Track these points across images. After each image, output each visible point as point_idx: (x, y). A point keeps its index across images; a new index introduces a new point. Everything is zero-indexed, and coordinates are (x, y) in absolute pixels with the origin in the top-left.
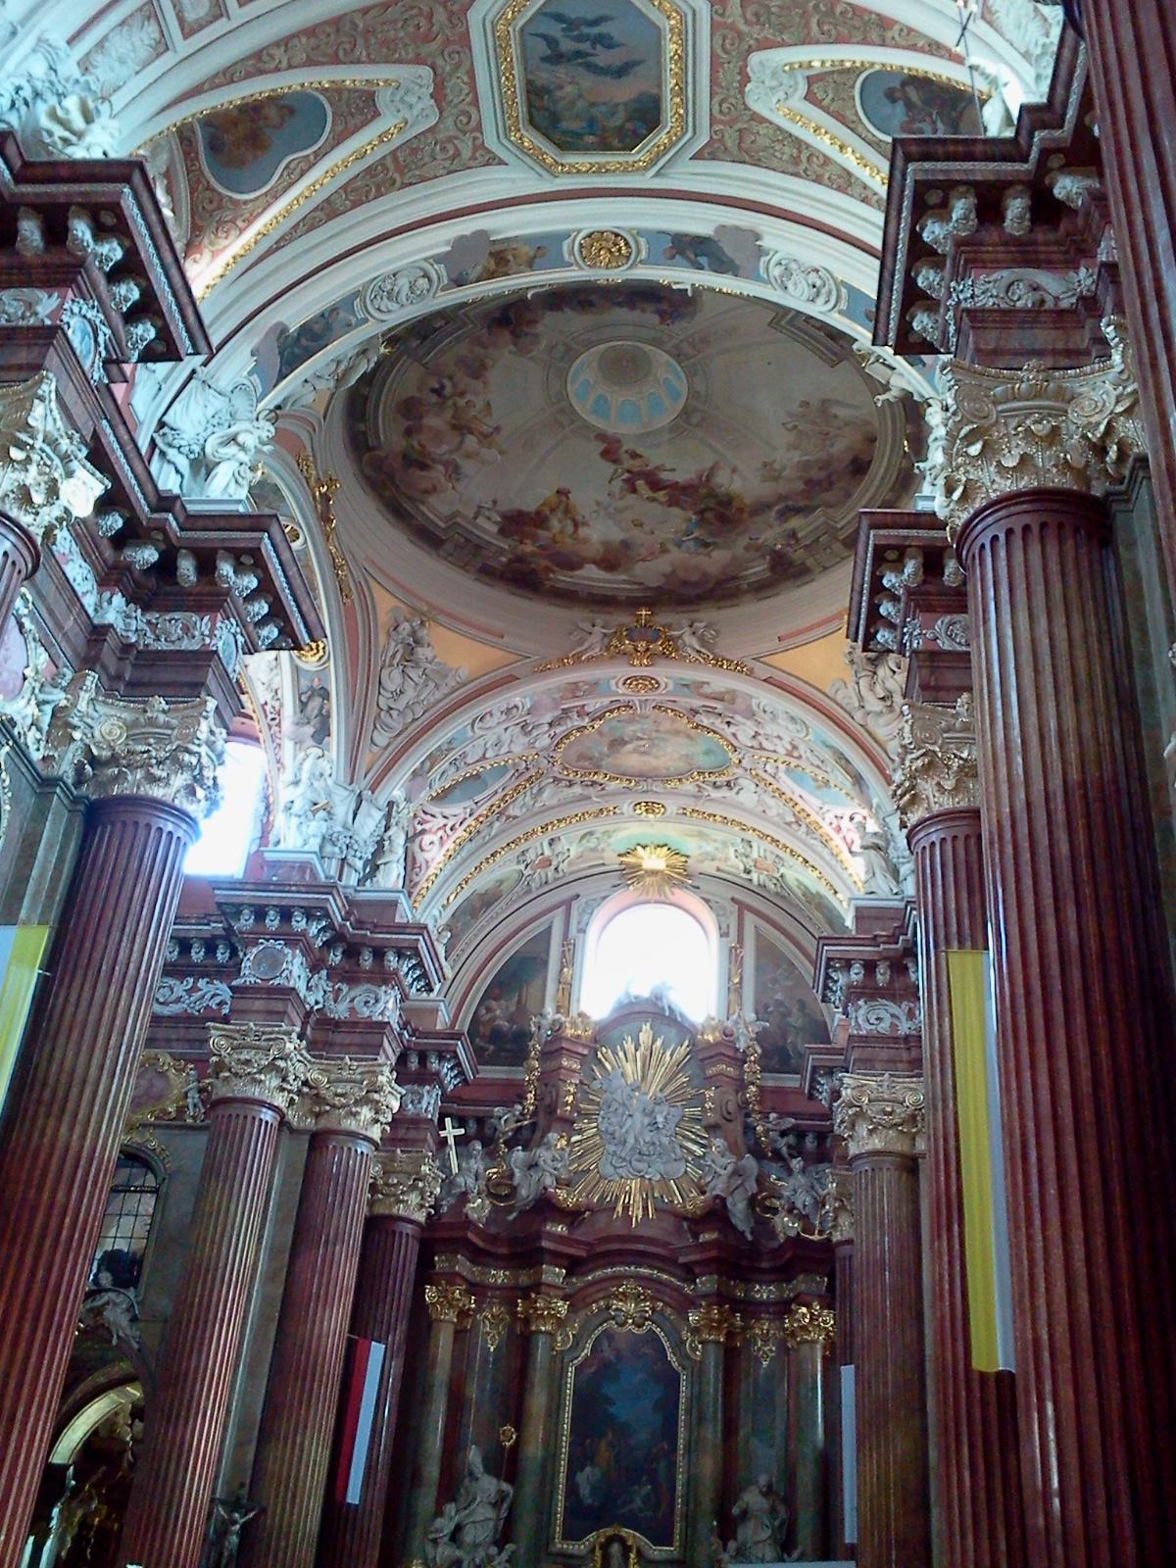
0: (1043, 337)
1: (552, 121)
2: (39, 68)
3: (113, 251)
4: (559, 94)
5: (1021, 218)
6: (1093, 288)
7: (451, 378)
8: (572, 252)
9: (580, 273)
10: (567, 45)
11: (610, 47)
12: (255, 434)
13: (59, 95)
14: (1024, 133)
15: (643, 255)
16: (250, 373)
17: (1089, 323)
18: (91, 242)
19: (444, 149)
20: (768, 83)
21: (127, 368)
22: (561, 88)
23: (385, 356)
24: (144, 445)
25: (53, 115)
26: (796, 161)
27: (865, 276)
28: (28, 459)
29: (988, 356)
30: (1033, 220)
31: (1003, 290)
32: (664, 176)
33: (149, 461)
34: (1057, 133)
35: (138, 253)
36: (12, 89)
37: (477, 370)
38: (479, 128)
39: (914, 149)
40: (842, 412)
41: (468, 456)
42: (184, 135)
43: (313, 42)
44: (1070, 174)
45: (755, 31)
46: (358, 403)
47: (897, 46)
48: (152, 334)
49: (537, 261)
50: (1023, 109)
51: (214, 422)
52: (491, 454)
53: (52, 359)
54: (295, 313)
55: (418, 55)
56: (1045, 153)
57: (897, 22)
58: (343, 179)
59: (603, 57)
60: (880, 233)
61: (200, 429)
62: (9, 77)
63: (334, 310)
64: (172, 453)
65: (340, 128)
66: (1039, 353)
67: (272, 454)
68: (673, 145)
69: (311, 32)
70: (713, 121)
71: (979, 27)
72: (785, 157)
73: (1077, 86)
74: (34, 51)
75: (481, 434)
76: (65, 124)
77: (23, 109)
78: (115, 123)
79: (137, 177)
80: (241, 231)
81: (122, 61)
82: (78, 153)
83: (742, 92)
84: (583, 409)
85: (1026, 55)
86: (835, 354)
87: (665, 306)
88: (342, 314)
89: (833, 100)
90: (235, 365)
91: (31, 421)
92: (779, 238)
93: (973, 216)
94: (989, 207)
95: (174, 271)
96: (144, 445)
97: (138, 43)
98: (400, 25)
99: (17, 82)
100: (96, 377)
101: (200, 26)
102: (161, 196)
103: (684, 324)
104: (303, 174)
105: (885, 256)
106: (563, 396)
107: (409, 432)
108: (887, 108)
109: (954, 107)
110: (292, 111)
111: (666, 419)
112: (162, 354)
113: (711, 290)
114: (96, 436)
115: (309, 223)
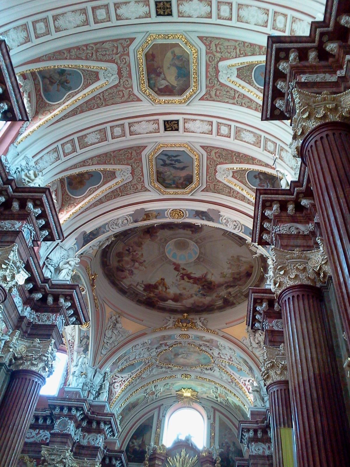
0: (299, 242)
1: (162, 180)
2: (24, 163)
3: (39, 211)
4: (165, 174)
7: (132, 247)
8: (167, 214)
10: (168, 162)
12: (74, 261)
15: (187, 216)
16: (75, 244)
18: (33, 209)
21: (39, 243)
23: (114, 240)
24: (41, 264)
26: (230, 193)
28: (7, 268)
29: (284, 247)
37: (140, 245)
39: (262, 191)
40: (243, 259)
41: (136, 268)
42: (62, 181)
44: (305, 199)
46: (105, 253)
47: (257, 165)
48: (47, 233)
50: (291, 182)
51: (63, 258)
53: (18, 240)
54: (88, 229)
56: (298, 194)
59: (178, 165)
61: (58, 260)
63: (100, 228)
64: (49, 266)
66: (299, 246)
67: (79, 267)
69: (99, 156)
71: (279, 161)
74: (23, 159)
78: (43, 178)
79: (47, 192)
80: (75, 206)
82: (32, 185)
83: (215, 175)
85: (292, 168)
87: (193, 229)
88: (102, 229)
90: (70, 242)
91: (9, 257)
92: (225, 213)
93: (279, 209)
94: (283, 206)
96: (41, 264)
97: (51, 158)
100: (30, 245)
101: (69, 154)
102: (54, 196)
103: (199, 234)
105: (255, 218)
106: (164, 252)
110: (92, 176)
111: (193, 260)
114: (28, 261)
115: (95, 205)
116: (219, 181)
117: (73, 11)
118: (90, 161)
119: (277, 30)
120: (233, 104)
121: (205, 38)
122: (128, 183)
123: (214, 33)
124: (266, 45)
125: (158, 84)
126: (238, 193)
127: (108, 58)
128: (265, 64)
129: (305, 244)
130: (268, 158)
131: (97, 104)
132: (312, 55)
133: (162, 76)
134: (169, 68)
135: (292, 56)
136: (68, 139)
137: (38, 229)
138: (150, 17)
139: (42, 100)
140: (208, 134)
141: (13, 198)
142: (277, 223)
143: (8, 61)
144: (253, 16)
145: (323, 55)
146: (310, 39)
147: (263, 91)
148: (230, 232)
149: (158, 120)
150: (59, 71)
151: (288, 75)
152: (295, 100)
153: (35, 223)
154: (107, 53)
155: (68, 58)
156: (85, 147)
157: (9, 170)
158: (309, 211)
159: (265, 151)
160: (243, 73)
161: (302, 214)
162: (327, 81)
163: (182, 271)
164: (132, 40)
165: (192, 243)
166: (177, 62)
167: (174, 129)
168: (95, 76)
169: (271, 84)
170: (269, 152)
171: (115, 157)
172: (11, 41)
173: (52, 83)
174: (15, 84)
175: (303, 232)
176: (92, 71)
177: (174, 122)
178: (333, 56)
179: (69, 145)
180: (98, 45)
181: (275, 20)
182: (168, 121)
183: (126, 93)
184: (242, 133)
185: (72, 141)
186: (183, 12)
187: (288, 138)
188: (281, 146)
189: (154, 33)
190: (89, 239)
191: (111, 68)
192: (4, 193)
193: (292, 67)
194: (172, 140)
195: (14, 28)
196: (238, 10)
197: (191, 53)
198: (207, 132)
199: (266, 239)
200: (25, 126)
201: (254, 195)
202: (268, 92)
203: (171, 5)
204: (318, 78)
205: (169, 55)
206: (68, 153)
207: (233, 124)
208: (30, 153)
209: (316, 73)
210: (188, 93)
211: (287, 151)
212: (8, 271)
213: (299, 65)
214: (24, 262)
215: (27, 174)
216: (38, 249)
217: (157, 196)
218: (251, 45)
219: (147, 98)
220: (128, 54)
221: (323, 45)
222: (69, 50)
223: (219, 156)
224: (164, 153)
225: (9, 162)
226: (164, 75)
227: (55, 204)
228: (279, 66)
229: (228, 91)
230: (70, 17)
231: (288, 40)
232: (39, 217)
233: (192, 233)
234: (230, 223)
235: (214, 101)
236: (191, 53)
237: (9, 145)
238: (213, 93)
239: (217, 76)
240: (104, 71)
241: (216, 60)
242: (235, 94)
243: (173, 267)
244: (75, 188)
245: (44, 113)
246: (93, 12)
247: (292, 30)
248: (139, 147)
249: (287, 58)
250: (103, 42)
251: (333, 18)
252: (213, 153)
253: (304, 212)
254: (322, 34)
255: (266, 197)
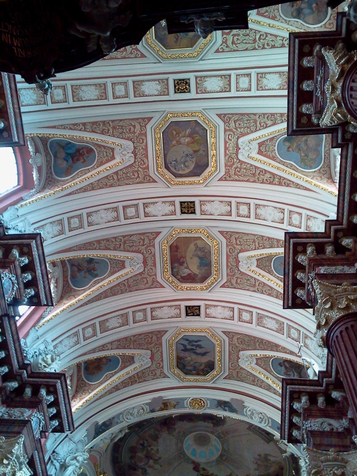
0: (334, 441)
1: (183, 366)
2: (42, 347)
3: (51, 398)
4: (186, 359)
5: (323, 403)
6: (348, 425)
7: (147, 441)
8: (187, 404)
9: (190, 410)
10: (189, 347)
11: (201, 348)
12: (82, 457)
13: (46, 354)
14: (320, 379)
15: (209, 406)
16: (85, 437)
17: (349, 437)
18: (45, 395)
19: (152, 373)
20: (245, 359)
21: (47, 434)
22: (187, 358)
23: (127, 433)
24: (46, 458)
25: (43, 360)
26: (254, 381)
27: (277, 417)
28: (9, 464)
29: (317, 446)
30: (326, 404)
31: (320, 424)
32: (216, 383)
33: (47, 464)
34: (330, 379)
35: (58, 400)
36: (33, 352)
37: (156, 438)
38: (162, 367)
39: (289, 382)
40: (272, 459)
41: (150, 467)
42: (78, 366)
43: (119, 343)
44: (336, 391)
45: (241, 346)
46: (117, 447)
47: (281, 352)
48: (57, 424)
49: (177, 406)
50: (319, 372)
51: (70, 452)
52: (157, 466)
53: (25, 431)
54: (101, 419)
55: (147, 347)
56: (328, 385)
57: (280, 346)
58: (121, 380)
59: (199, 350)
60: (280, 403)
61: (65, 454)
62: (34, 349)
63: (113, 418)
64: (55, 462)
65: (123, 366)
66: (335, 446)
67: (87, 464)
68: (218, 375)
69: (118, 340)
70: (229, 369)
71: (304, 348)
72: (251, 380)
73: (334, 367)
74: (42, 343)
75: (155, 459)
76: (45, 362)
77: (35, 357)
78: (60, 362)
79: (63, 378)
80: (90, 393)
81: (65, 346)
82: (47, 370)
83: (238, 362)
84: (188, 453)
85: (318, 356)
86: (268, 439)
87: (215, 421)
88: (116, 420)
89: (264, 365)
90: (80, 434)
91: (13, 451)
92: (249, 403)
93: (308, 402)
94: (313, 398)
95: (68, 405)
96: (46, 458)
97: (71, 341)
98: (143, 340)
99: (35, 350)
100: (37, 437)
101: (89, 338)
102: (68, 382)
103: (221, 427)
104: (111, 377)
105: (283, 410)
106: (182, 448)
107: (132, 458)
108: (279, 368)
109: (299, 369)
110: (110, 361)
111: (214, 458)
112: (59, 430)
113: (229, 417)
114: (32, 456)
115: (110, 392)
116: (242, 369)
117: (105, 210)
118: (109, 346)
119: (293, 226)
120: (254, 291)
121: (225, 232)
122: (147, 368)
123: (233, 228)
124: (284, 239)
125: (181, 273)
126: (263, 381)
127: (134, 248)
128: (283, 255)
129: (340, 444)
130: (292, 346)
131: (121, 290)
132: (329, 249)
133: (185, 265)
134: (191, 258)
135: (309, 250)
136: (90, 324)
137: (47, 419)
138: (175, 215)
139: (69, 286)
140: (229, 319)
141: (27, 384)
142: (313, 268)
143: (41, 251)
144: (270, 215)
145: (339, 249)
146: (326, 235)
147: (283, 280)
148: (256, 426)
149: (180, 305)
150: (88, 259)
151: (307, 267)
152: (316, 291)
153: (19, 276)
154: (135, 244)
155: (97, 248)
156: (106, 331)
157: (26, 354)
158: (341, 405)
159: (288, 338)
160: (263, 263)
161: (334, 409)
162: (346, 273)
163: (202, 472)
164: (158, 233)
165: (213, 437)
166: (199, 253)
167: (195, 314)
168: (122, 264)
169: (291, 274)
170: (293, 339)
171: (135, 341)
172: (46, 233)
173: (80, 270)
174: (44, 272)
175: (337, 428)
176: (119, 260)
177: (196, 308)
178: (350, 250)
179: (90, 330)
180: (126, 238)
181: (290, 218)
182: (189, 307)
183: (150, 280)
184: (264, 320)
185: (94, 325)
186: (205, 210)
187: (313, 327)
188: (305, 334)
189: (178, 228)
190: (100, 430)
191: (137, 258)
192: (18, 378)
193: (310, 260)
194: (194, 325)
195: (51, 223)
196: (256, 209)
197: (212, 245)
198: (229, 318)
199: (297, 436)
200: (48, 310)
201: (281, 384)
202: (288, 282)
203: (194, 205)
204: (338, 270)
205: (192, 247)
206: (88, 337)
207: (254, 311)
208: (49, 337)
209: (334, 265)
210: (209, 281)
211: (311, 339)
212: (10, 467)
213: (317, 257)
214: (28, 458)
215: (44, 358)
216: (46, 442)
217: (175, 383)
218: (269, 238)
219: (170, 284)
220: (154, 246)
221: (338, 240)
222: (99, 242)
223: (241, 342)
224: (185, 338)
225: (28, 345)
226: (187, 264)
227: (69, 390)
228: (297, 258)
229: (248, 280)
230: (103, 214)
231: (304, 235)
232: (50, 406)
233: (214, 426)
234: (256, 415)
235: (235, 288)
236: (212, 245)
237: (31, 329)
238: (234, 281)
239: (237, 266)
240: (130, 260)
241: (236, 252)
242: (255, 282)
243: (191, 466)
244: (92, 374)
245: (69, 298)
246: (124, 210)
247: (307, 227)
248: (159, 332)
249: (304, 252)
250: (131, 235)
251: (345, 218)
252: (235, 339)
253: (336, 405)
254: (336, 231)
255: (293, 388)
